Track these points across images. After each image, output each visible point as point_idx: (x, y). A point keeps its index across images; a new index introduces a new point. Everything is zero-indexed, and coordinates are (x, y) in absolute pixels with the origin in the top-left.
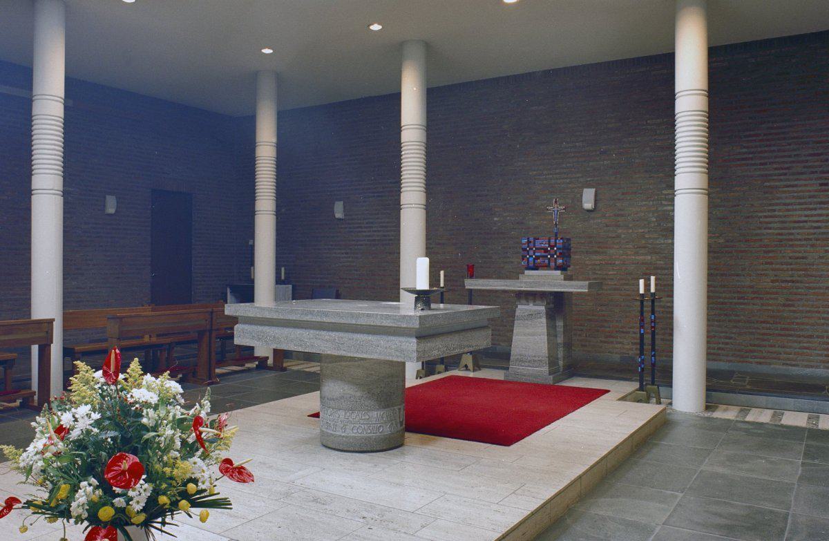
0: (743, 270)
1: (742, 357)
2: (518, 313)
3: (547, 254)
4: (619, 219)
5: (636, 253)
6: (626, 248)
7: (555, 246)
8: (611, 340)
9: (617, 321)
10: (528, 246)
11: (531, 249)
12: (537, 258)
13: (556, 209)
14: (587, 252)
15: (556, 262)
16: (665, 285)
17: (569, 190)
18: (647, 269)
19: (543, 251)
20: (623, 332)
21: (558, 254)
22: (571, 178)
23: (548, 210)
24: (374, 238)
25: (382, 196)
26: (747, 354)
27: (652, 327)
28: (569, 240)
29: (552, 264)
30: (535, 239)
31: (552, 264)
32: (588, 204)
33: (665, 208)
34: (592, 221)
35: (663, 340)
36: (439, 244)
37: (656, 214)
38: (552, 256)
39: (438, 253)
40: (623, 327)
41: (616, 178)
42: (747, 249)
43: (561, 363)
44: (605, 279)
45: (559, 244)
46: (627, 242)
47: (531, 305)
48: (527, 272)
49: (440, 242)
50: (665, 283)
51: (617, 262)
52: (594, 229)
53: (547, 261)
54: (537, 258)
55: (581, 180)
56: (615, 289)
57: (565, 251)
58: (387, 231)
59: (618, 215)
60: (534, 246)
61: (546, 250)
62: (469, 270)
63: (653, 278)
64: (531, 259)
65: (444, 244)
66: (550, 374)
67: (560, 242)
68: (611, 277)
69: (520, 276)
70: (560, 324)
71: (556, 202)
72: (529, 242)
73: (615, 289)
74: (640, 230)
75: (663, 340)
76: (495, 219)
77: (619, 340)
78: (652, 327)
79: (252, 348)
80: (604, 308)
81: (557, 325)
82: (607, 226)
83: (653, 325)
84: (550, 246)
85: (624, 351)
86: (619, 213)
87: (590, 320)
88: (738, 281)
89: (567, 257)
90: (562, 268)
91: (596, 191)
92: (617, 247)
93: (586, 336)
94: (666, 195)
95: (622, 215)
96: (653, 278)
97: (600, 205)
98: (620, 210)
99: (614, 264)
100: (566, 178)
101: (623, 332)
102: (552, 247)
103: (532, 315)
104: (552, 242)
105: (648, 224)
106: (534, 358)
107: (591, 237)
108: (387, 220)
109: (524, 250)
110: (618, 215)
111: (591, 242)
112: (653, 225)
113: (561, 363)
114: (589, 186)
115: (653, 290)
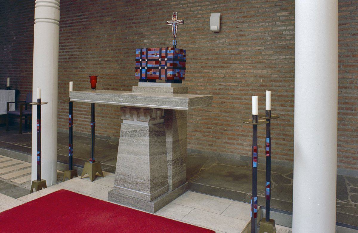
0: (351, 83)
1: (350, 163)
2: (123, 128)
3: (158, 65)
4: (240, 38)
5: (255, 68)
6: (246, 63)
7: (166, 57)
8: (233, 141)
9: (238, 126)
10: (141, 58)
11: (144, 60)
12: (149, 69)
13: (174, 22)
14: (214, 67)
15: (166, 74)
16: (279, 96)
17: (200, 16)
18: (264, 81)
19: (154, 62)
20: (243, 136)
21: (168, 65)
22: (202, 6)
23: (167, 23)
24: (66, 57)
25: (71, 26)
26: (355, 161)
27: (267, 152)
28: (182, 51)
29: (163, 76)
30: (148, 50)
31: (163, 76)
32: (214, 26)
33: (279, 28)
34: (218, 41)
35: (276, 144)
36: (106, 61)
37: (271, 34)
38: (163, 67)
39: (105, 68)
40: (243, 131)
41: (237, 4)
42: (354, 64)
43: (170, 181)
44: (228, 90)
45: (170, 54)
46: (246, 58)
47: (135, 120)
48: (141, 84)
49: (107, 59)
50: (279, 94)
51: (238, 76)
52: (220, 47)
53: (158, 73)
54: (149, 69)
55: (210, 7)
56: (236, 99)
58: (74, 52)
59: (240, 35)
60: (147, 57)
61: (157, 62)
62: (91, 81)
63: (268, 94)
64: (144, 71)
65: (109, 61)
66: (152, 200)
67: (170, 52)
68: (234, 88)
69: (134, 88)
70: (169, 139)
71: (174, 16)
72: (142, 53)
73: (236, 99)
74: (258, 48)
75: (276, 144)
76: (145, 41)
77: (239, 142)
78: (267, 152)
80: (227, 114)
81: (167, 140)
82: (230, 45)
83: (268, 149)
84: (161, 57)
85: (244, 152)
86: (241, 33)
87: (216, 124)
88: (346, 93)
89: (179, 68)
90: (175, 80)
91: (221, 16)
92: (239, 62)
93: (213, 137)
94: (280, 17)
95: (242, 36)
96: (268, 94)
97: (224, 27)
98: (241, 31)
99: (236, 76)
101: (243, 136)
102: (163, 58)
103: (135, 131)
104: (163, 53)
105: (265, 43)
106: (136, 180)
107: (216, 54)
108: (74, 43)
109: (138, 61)
110: (240, 35)
111: (217, 58)
112: (268, 43)
113: (170, 181)
114: (216, 12)
115: (268, 107)
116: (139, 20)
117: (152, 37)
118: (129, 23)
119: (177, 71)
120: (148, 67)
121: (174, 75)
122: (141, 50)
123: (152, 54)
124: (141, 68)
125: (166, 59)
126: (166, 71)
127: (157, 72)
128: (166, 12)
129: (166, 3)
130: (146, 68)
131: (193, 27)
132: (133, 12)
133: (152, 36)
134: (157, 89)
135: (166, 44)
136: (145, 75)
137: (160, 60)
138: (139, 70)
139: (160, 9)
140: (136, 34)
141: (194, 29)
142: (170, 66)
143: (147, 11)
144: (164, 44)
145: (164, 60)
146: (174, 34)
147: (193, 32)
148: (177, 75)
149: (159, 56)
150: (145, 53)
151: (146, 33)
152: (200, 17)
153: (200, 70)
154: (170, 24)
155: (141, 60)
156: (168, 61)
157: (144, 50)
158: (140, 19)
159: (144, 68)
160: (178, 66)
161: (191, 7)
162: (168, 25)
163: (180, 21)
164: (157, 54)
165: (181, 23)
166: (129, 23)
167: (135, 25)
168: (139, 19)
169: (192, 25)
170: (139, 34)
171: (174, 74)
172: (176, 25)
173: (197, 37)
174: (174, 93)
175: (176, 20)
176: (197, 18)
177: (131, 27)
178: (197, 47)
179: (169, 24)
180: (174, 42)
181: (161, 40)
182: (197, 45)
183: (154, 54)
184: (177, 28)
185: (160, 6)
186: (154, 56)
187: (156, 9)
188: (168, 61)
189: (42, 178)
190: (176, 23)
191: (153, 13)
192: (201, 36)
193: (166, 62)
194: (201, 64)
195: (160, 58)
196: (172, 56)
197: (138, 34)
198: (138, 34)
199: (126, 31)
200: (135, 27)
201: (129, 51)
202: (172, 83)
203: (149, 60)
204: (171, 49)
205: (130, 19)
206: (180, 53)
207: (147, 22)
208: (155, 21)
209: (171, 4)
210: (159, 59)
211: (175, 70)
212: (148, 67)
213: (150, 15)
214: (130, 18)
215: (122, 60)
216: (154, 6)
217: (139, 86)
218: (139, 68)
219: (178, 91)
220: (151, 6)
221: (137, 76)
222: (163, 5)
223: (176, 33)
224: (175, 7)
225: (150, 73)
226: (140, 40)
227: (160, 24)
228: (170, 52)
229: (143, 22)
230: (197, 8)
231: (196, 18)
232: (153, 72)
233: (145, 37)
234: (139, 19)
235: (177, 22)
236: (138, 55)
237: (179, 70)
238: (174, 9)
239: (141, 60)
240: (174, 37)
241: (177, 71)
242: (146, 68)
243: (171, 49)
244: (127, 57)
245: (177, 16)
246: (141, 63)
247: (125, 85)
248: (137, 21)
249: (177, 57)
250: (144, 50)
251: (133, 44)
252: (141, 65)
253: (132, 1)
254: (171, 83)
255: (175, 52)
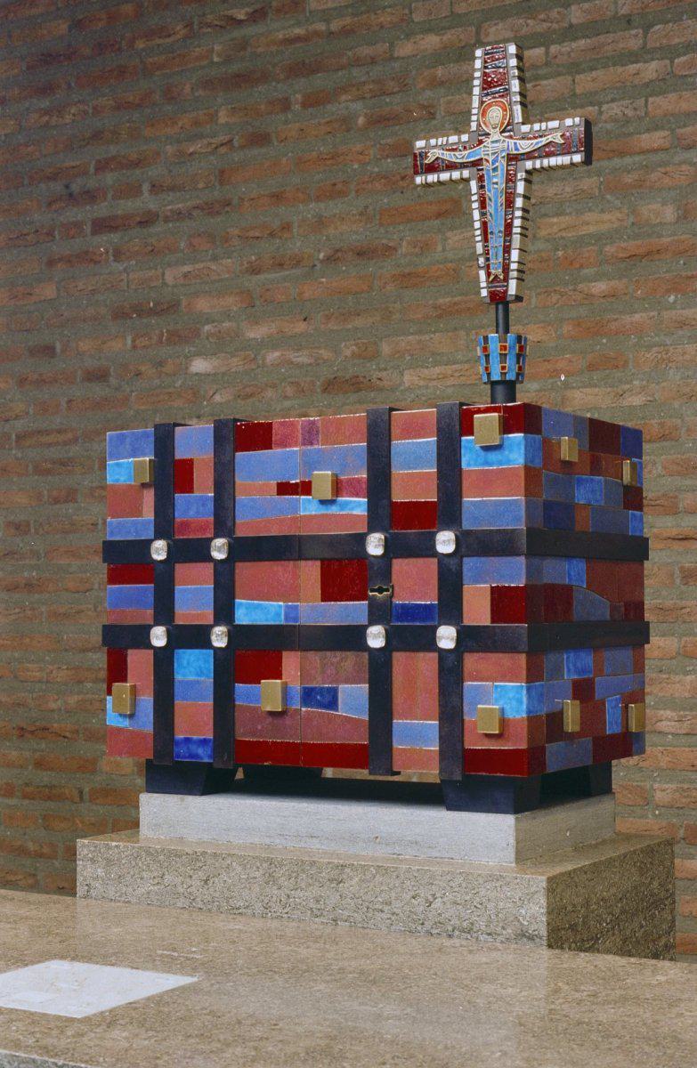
3: (350, 611)
10: (164, 526)
15: (451, 715)
17: (658, 138)
19: (310, 572)
21: (477, 609)
22: (670, 52)
45: (488, 481)
53: (354, 698)
57: (569, 572)
60: (223, 521)
64: (194, 668)
76: (200, 366)
79: (648, 559)
84: (387, 513)
89: (590, 637)
100: (634, 57)
102: (422, 518)
116: (147, 201)
117: (252, 335)
118: (74, 229)
119: (569, 676)
120: (236, 633)
121: (547, 725)
122: (164, 439)
123: (284, 489)
124: (159, 637)
125: (445, 542)
126: (451, 672)
127: (342, 687)
128: (361, 121)
129: (365, 51)
130: (219, 638)
131: (599, 238)
132: (97, 136)
133: (255, 321)
134: (352, 884)
135: (371, 387)
136: (208, 717)
137: (375, 546)
138: (139, 663)
139: (314, 101)
140: (120, 314)
141: (610, 249)
142: (498, 612)
143: (213, 117)
144: (356, 385)
145: (430, 551)
146: (497, 270)
147: (597, 278)
148: (571, 722)
149: (357, 506)
150: (204, 479)
151: (203, 305)
152: (655, 151)
153: (669, 603)
154: (451, 166)
155: (159, 551)
156: (469, 564)
157: (195, 443)
158: (156, 188)
159: (195, 637)
160: (579, 612)
161: (574, 68)
162: (432, 178)
163: (556, 128)
164: (338, 487)
165: (566, 149)
166: (74, 229)
167: (115, 237)
168: (146, 187)
169: (588, 216)
170: (153, 312)
171: (543, 710)
172: (511, 179)
173: (637, 317)
174: (556, 939)
175: (507, 128)
176: (628, 160)
177: (87, 257)
178: (637, 401)
179: (432, 168)
180: (495, 346)
181: (325, 354)
182: (643, 388)
183: (306, 488)
184: (519, 202)
185: (314, 72)
186: (307, 506)
187: (285, 105)
188: (469, 564)
189: (177, 428)
190: (513, 158)
191: (260, 139)
192: (673, 306)
193: (450, 582)
194: (677, 546)
195: (372, 528)
196: (520, 498)
197: (140, 311)
198: (140, 311)
199: (49, 291)
200: (118, 254)
201: (74, 450)
202: (517, 810)
203: (251, 549)
204: (507, 427)
205: (71, 195)
206: (595, 468)
207: (210, 209)
208: (277, 197)
209: (405, 49)
210: (360, 539)
211: (550, 660)
212: (236, 633)
213: (237, 156)
214: (75, 188)
215: (17, 527)
216: (264, 77)
217: (145, 830)
218: (139, 636)
219: (587, 904)
220: (243, 80)
221: (125, 724)
222: (342, 68)
223: (515, 255)
224: (440, 72)
225: (267, 695)
226: (161, 364)
227: (320, 223)
228: (495, 462)
229: (179, 215)
230: (632, 68)
231: (622, 154)
232: (296, 687)
233: (196, 333)
234: (146, 187)
235: (525, 146)
236: (124, 501)
237: (587, 659)
238: (428, 93)
239: (159, 551)
240: (498, 298)
241: (572, 665)
242: (219, 638)
243: (507, 427)
244: (56, 501)
245: (515, 86)
246: (163, 581)
247: (45, 729)
248: (127, 206)
249: (569, 508)
250: (195, 443)
251: (98, 391)
252: (164, 611)
253: (87, 51)
254: (509, 820)
255: (548, 449)
